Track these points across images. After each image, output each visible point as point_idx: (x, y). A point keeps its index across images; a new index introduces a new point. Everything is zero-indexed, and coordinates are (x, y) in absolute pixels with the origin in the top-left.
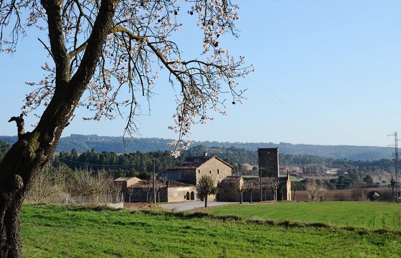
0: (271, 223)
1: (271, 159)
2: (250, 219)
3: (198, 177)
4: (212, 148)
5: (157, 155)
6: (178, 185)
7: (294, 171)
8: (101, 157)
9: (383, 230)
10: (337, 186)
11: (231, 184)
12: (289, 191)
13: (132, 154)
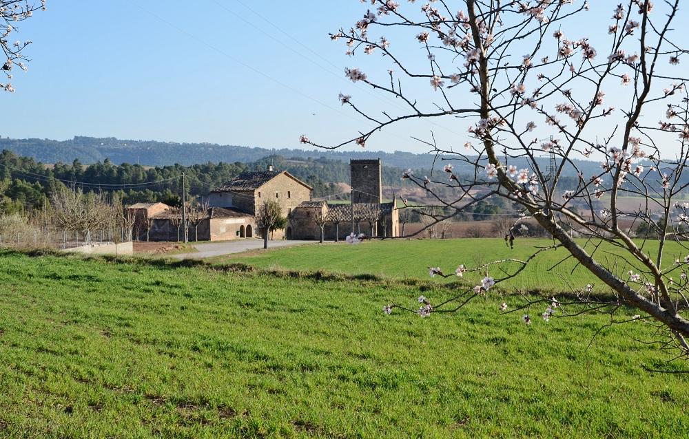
0: (294, 275)
1: (369, 176)
2: (265, 269)
3: (258, 203)
4: (293, 159)
5: (206, 169)
6: (227, 216)
7: (414, 194)
8: (120, 171)
9: (457, 283)
10: (474, 216)
11: (308, 213)
12: (396, 224)
13: (168, 168)
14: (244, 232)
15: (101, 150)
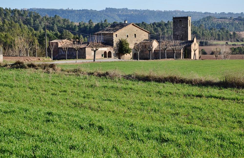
1: (183, 26)
3: (116, 40)
4: (221, 18)
5: (159, 25)
14: (107, 55)
15: (119, 16)
